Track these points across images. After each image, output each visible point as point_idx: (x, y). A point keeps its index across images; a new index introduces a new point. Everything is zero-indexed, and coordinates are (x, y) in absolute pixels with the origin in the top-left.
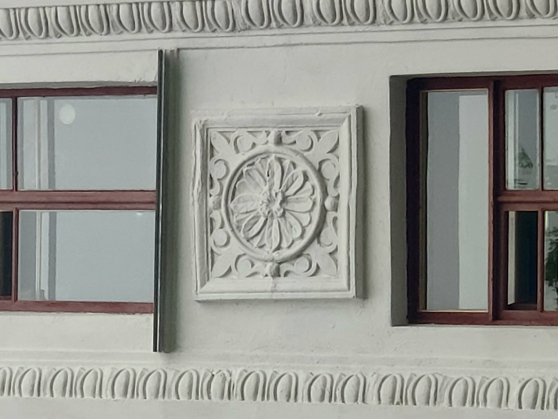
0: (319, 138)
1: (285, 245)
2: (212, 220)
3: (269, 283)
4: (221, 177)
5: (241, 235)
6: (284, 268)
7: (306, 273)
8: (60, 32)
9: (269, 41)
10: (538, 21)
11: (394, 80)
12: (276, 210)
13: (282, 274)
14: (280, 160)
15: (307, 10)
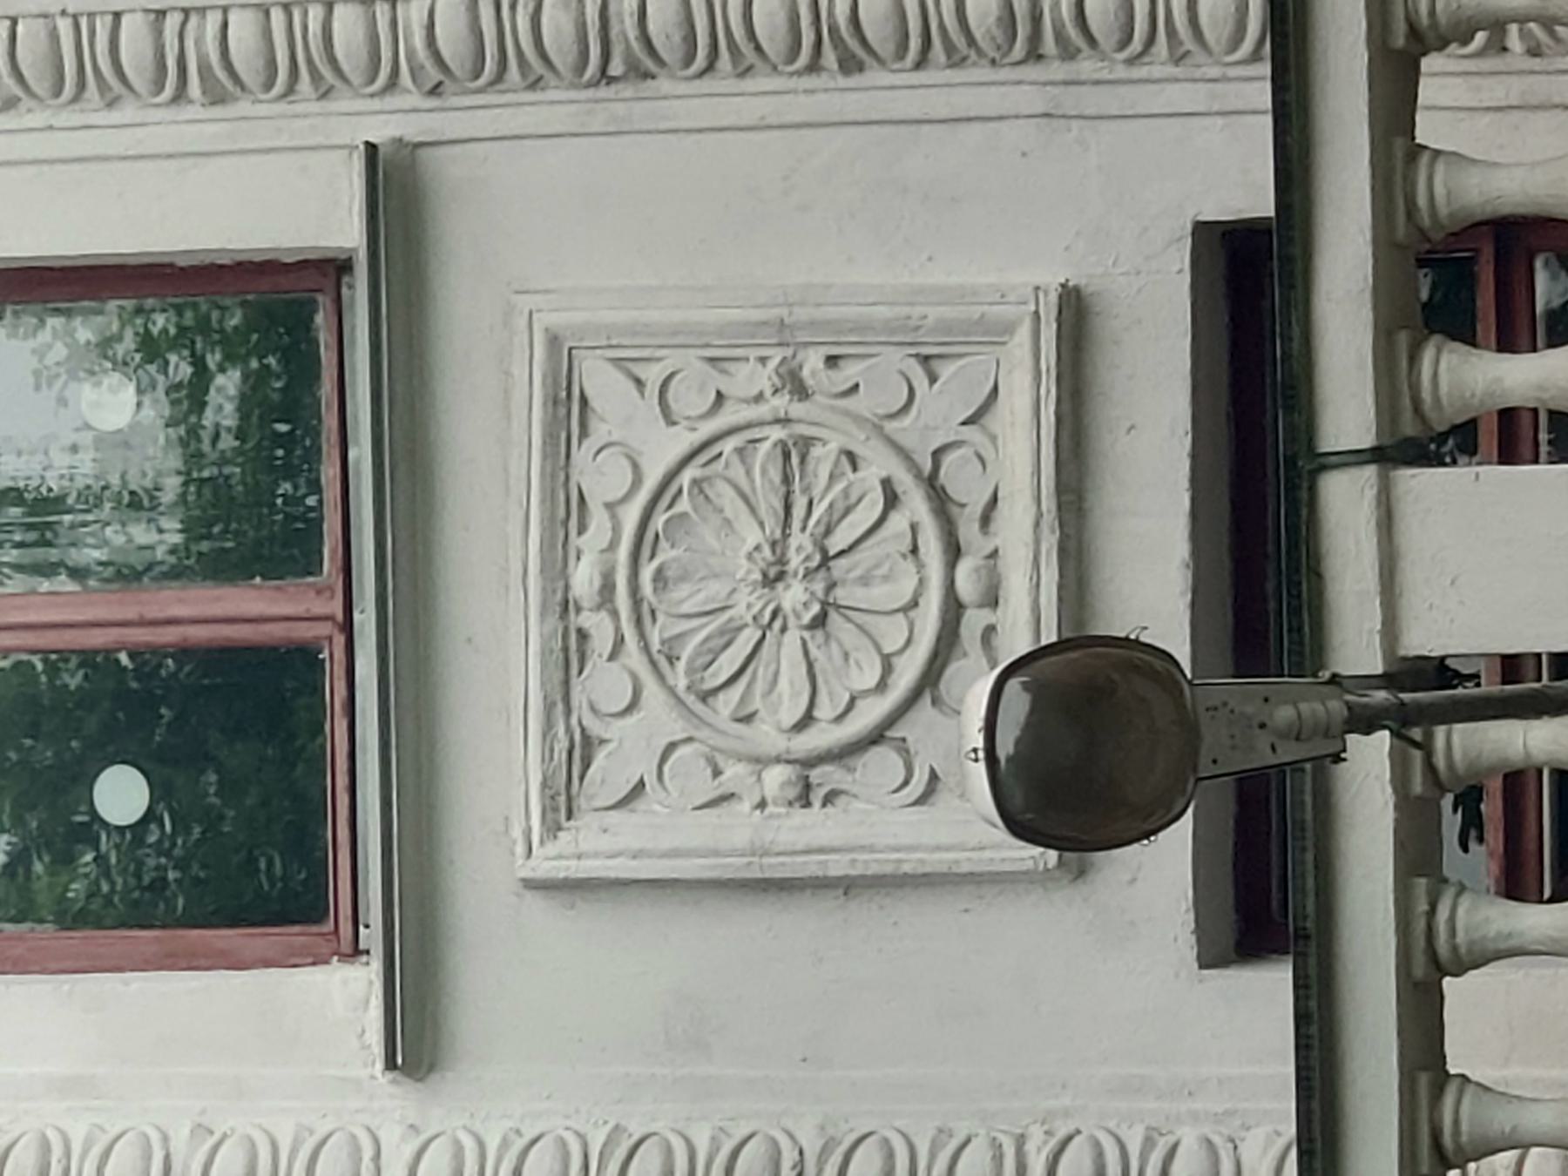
0: (933, 379)
1: (824, 711)
2: (583, 635)
4: (612, 496)
7: (896, 795)
11: (1203, 231)
12: (799, 607)
13: (817, 797)
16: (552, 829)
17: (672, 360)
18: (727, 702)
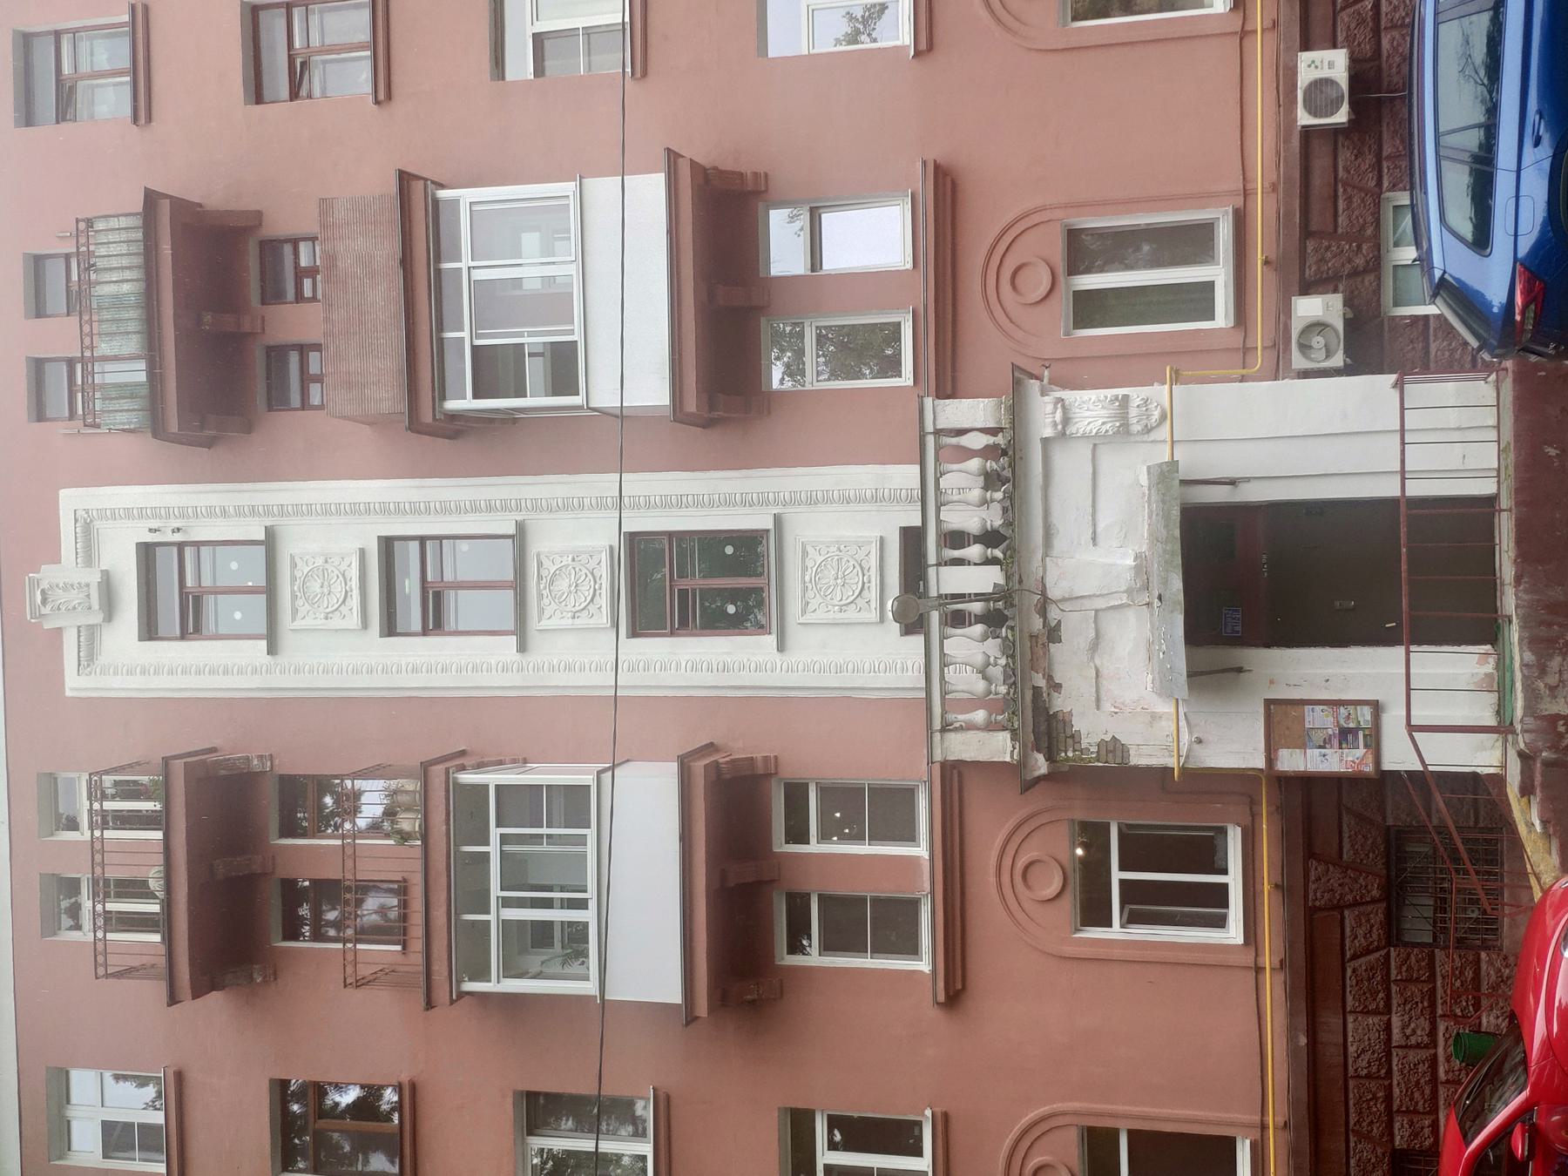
1: (844, 598)
3: (570, 621)
5: (557, 601)
6: (577, 615)
8: (466, 512)
9: (897, 508)
10: (690, 509)
14: (574, 568)
15: (585, 504)
16: (802, 616)
17: (821, 546)
18: (563, 604)
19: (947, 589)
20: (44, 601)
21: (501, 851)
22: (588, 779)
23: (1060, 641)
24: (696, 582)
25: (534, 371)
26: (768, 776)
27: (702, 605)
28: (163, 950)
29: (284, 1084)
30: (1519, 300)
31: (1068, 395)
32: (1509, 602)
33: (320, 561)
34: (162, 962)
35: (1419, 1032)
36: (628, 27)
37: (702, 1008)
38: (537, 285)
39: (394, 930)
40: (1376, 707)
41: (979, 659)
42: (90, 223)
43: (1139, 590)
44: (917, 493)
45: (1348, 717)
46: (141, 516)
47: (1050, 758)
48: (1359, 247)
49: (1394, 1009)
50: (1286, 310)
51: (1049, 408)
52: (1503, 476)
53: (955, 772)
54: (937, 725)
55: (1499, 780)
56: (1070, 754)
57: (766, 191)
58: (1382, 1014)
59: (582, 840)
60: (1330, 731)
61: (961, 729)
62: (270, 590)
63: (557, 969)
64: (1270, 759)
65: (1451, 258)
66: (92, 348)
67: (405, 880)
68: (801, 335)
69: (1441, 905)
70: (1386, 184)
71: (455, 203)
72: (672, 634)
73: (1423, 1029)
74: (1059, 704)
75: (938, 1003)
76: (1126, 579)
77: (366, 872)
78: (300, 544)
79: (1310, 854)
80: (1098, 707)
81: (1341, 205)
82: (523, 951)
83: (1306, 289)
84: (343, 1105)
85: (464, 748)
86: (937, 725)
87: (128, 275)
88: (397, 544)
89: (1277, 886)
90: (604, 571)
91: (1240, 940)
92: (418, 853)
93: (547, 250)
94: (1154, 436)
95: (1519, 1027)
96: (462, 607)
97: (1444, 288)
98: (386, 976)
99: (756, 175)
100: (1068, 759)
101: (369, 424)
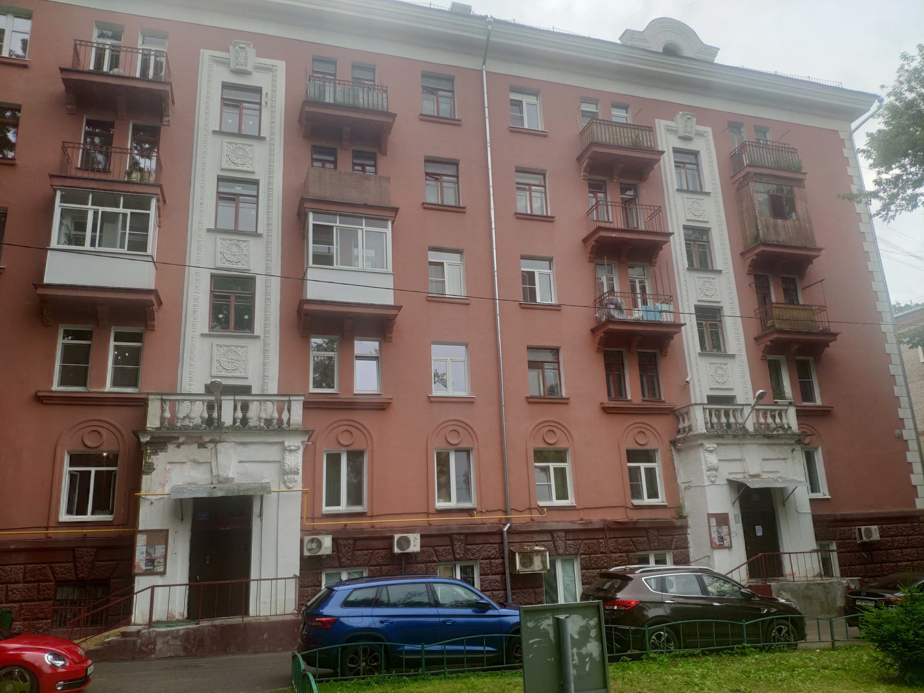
8: (268, 215)
19: (224, 403)
20: (240, 47)
21: (120, 213)
22: (149, 252)
23: (198, 448)
24: (233, 303)
25: (323, 248)
26: (146, 326)
27: (224, 304)
28: (86, 69)
29: (19, 111)
30: (324, 619)
31: (301, 452)
32: (205, 623)
33: (251, 156)
34: (80, 68)
35: (14, 595)
36: (442, 296)
37: (40, 291)
38: (355, 254)
39: (88, 163)
40: (163, 573)
41: (193, 415)
42: (386, 91)
43: (218, 479)
44: (265, 393)
45: (159, 562)
46: (273, 90)
47: (147, 443)
48: (349, 559)
49: (26, 585)
50: (327, 533)
51: (296, 444)
52: (256, 618)
53: (143, 404)
54: (164, 397)
55: (128, 623)
56: (149, 451)
57: (385, 341)
58: (24, 579)
59: (122, 246)
60: (153, 555)
61: (162, 407)
62: (240, 135)
63: (64, 230)
64: (142, 532)
65: (341, 593)
66: (339, 84)
67: (110, 172)
68: (333, 351)
69: (73, 603)
70: (371, 568)
71: (386, 227)
72: (211, 291)
73: (15, 597)
74: (171, 447)
75: (37, 392)
76: (223, 474)
77: (115, 158)
78: (258, 151)
79: (99, 549)
80: (169, 463)
81: (365, 552)
82: (73, 218)
83: (334, 540)
84: (8, 134)
85: (167, 202)
86: (164, 397)
87: (366, 102)
88: (256, 186)
89: (85, 535)
90: (239, 266)
91: (60, 520)
92: (121, 179)
93: (368, 259)
94: (282, 485)
95: (13, 637)
96: (228, 209)
97: (330, 590)
98: (66, 160)
99: (391, 338)
100: (146, 450)
101: (305, 183)
